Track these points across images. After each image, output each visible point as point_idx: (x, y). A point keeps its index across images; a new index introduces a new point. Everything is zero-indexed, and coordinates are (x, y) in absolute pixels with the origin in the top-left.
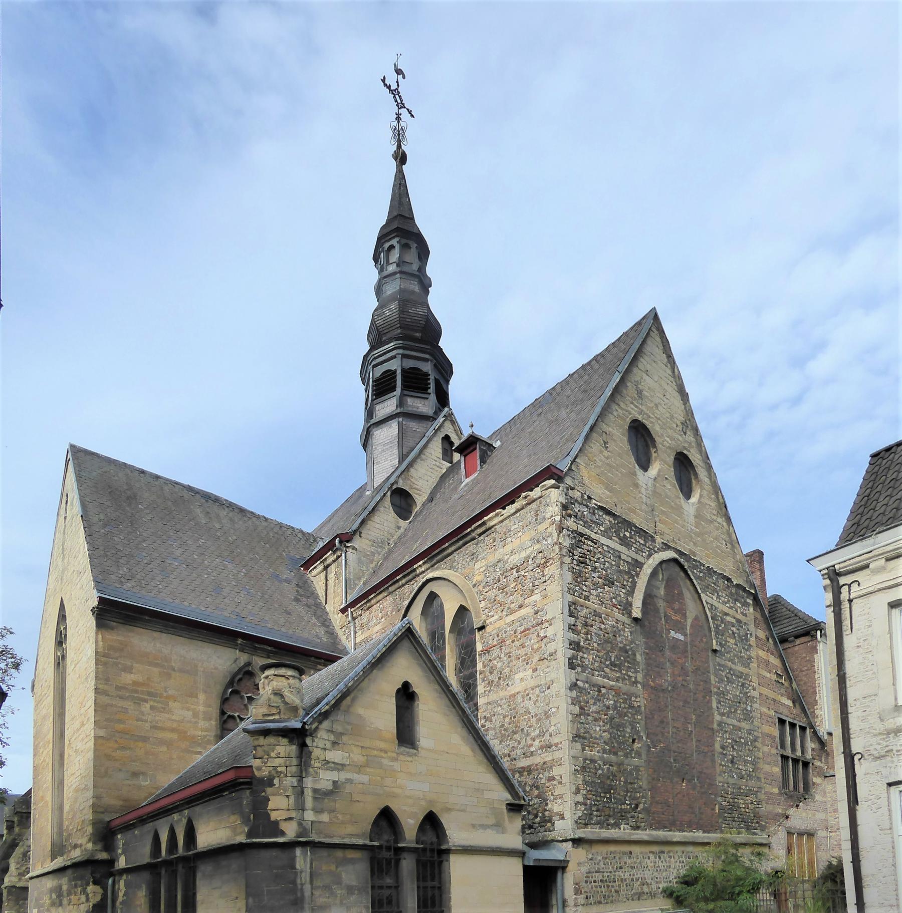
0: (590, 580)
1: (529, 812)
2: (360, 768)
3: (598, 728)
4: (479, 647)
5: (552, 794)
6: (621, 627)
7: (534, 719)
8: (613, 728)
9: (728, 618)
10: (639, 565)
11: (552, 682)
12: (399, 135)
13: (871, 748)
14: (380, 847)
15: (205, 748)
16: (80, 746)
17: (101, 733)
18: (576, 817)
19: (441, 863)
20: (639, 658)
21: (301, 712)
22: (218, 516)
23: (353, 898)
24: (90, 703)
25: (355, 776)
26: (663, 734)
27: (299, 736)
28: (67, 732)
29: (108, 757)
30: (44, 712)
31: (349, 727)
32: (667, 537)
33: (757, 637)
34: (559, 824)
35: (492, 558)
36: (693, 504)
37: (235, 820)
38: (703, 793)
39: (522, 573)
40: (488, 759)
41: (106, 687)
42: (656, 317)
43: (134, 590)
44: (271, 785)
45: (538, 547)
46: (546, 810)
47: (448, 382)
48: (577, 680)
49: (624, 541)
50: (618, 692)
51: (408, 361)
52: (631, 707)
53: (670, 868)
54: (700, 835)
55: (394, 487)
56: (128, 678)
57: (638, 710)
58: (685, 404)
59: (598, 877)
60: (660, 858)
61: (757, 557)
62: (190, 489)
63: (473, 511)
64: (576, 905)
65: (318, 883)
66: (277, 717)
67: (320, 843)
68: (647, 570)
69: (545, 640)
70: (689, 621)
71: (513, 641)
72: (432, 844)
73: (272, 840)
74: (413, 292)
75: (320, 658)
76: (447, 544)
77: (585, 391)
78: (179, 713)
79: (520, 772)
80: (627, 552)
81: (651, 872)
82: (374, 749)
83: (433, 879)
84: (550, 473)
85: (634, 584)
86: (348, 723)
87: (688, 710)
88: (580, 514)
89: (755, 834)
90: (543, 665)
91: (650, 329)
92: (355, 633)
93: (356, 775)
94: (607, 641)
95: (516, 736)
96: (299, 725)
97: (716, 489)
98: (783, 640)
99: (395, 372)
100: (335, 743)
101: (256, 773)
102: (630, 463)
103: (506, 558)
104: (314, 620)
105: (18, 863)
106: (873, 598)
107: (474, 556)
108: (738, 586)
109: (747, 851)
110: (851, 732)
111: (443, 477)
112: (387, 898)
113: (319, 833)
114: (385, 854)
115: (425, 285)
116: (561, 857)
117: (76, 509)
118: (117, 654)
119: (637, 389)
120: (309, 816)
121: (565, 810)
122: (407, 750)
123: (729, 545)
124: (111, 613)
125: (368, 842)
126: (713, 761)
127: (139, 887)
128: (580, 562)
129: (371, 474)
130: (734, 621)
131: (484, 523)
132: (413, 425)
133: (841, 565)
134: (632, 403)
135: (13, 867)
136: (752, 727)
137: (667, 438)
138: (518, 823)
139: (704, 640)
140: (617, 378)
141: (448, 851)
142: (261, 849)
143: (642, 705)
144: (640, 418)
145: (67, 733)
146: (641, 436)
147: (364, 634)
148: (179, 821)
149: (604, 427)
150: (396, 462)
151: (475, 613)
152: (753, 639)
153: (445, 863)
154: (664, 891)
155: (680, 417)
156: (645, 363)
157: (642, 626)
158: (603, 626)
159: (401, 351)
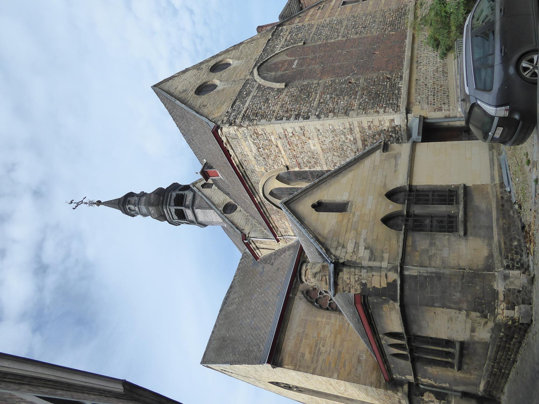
1: (389, 140)
2: (358, 234)
3: (342, 102)
4: (297, 169)
5: (379, 127)
7: (336, 138)
8: (342, 94)
9: (288, 38)
11: (316, 128)
12: (92, 203)
14: (406, 225)
15: (346, 321)
16: (342, 388)
17: (336, 375)
18: (393, 112)
19: (417, 191)
20: (305, 83)
21: (325, 263)
22: (233, 299)
23: (438, 243)
24: (320, 378)
25: (363, 237)
27: (338, 266)
29: (349, 374)
31: (335, 238)
33: (299, 22)
34: (397, 122)
35: (254, 162)
37: (386, 308)
38: (382, 42)
40: (356, 163)
42: (155, 86)
44: (365, 284)
45: (249, 138)
47: (180, 185)
50: (323, 93)
51: (171, 203)
52: (331, 85)
54: (408, 41)
56: (307, 356)
57: (333, 82)
58: (190, 70)
59: (431, 98)
61: (260, 29)
62: (221, 311)
64: (449, 110)
65: (427, 263)
66: (327, 277)
67: (401, 260)
69: (294, 133)
70: (288, 58)
71: (294, 150)
72: (405, 195)
73: (399, 288)
77: (183, 118)
78: (326, 332)
79: (365, 146)
83: (428, 196)
84: (215, 132)
86: (332, 239)
89: (409, 10)
90: (307, 134)
92: (289, 235)
93: (362, 236)
94: (296, 100)
95: (345, 148)
96: (332, 265)
97: (227, 51)
98: (301, 9)
100: (343, 247)
101: (359, 292)
104: (282, 256)
107: (253, 171)
108: (272, 35)
109: (419, 13)
111: (219, 188)
113: (395, 259)
114: (410, 223)
115: (143, 194)
118: (295, 359)
119: (182, 92)
120: (385, 264)
123: (253, 42)
124: (275, 358)
125: (402, 232)
127: (426, 371)
128: (257, 116)
129: (217, 224)
130: (289, 35)
131: (238, 166)
132: (197, 202)
136: (346, 19)
137: (204, 77)
138: (395, 146)
140: (178, 102)
141: (410, 186)
142: (403, 293)
143: (330, 79)
144: (194, 90)
145: (336, 393)
146: (203, 89)
147: (290, 231)
148: (386, 341)
152: (299, 24)
153: (418, 188)
154: (442, 58)
155: (195, 71)
157: (289, 82)
158: (288, 103)
159: (168, 206)
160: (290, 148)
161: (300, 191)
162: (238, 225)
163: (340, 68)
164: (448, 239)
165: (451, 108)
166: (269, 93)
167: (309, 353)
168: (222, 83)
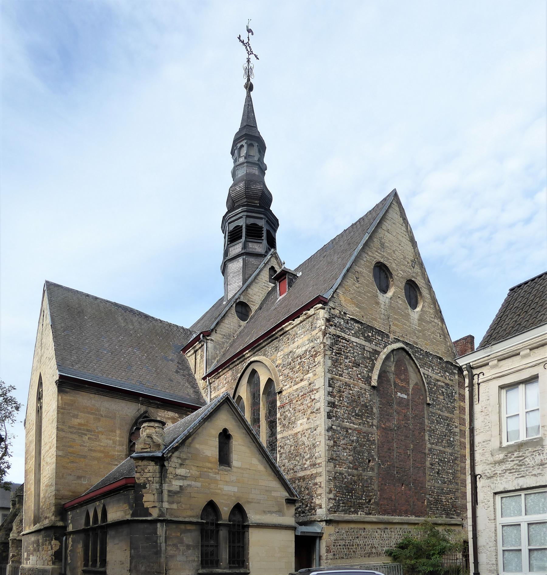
0: (343, 364)
1: (303, 504)
2: (195, 479)
3: (345, 454)
4: (278, 404)
6: (363, 392)
7: (307, 448)
9: (439, 383)
10: (378, 353)
11: (318, 426)
12: (248, 72)
13: (486, 472)
15: (120, 462)
16: (49, 460)
17: (60, 453)
18: (329, 507)
20: (375, 410)
21: (162, 447)
22: (132, 321)
23: (190, 552)
24: (54, 436)
26: (390, 457)
27: (160, 461)
28: (42, 452)
29: (64, 467)
30: (31, 439)
31: (190, 455)
32: (398, 334)
34: (319, 511)
35: (287, 350)
36: (417, 312)
37: (126, 507)
38: (416, 493)
39: (303, 360)
40: (275, 473)
41: (63, 427)
43: (80, 369)
45: (312, 344)
46: (312, 503)
48: (332, 425)
49: (368, 339)
50: (359, 432)
51: (251, 219)
52: (368, 440)
53: (393, 538)
54: (413, 518)
55: (238, 301)
56: (76, 421)
57: (373, 442)
58: (414, 248)
60: (384, 532)
62: (116, 304)
63: (310, 297)
65: (170, 542)
66: (149, 450)
67: (171, 520)
68: (383, 356)
70: (411, 386)
71: (297, 401)
72: (239, 522)
73: (144, 518)
74: (254, 174)
75: (189, 408)
76: (262, 341)
78: (105, 441)
80: (369, 346)
81: (378, 540)
82: (204, 468)
83: (239, 542)
84: (319, 300)
85: (373, 365)
86: (190, 453)
87: (408, 441)
88: (338, 324)
89: (452, 518)
90: (312, 416)
91: (392, 203)
92: (211, 392)
93: (193, 483)
94: (354, 401)
95: (297, 458)
96: (160, 455)
99: (242, 227)
100: (181, 465)
101: (137, 481)
102: (374, 290)
103: (294, 350)
104: (187, 384)
105: (17, 526)
106: (490, 383)
107: (277, 349)
110: (476, 462)
111: (269, 293)
112: (211, 552)
113: (171, 515)
114: (210, 527)
115: (263, 169)
116: (319, 531)
117: (48, 320)
118: (70, 408)
120: (166, 505)
121: (322, 503)
122: (225, 468)
124: (65, 384)
125: (200, 520)
126: (425, 473)
130: (443, 384)
132: (252, 260)
133: (474, 363)
134: (377, 252)
135: (14, 528)
137: (400, 273)
138: (292, 510)
139: (422, 398)
140: (366, 237)
141: (248, 526)
142: (139, 524)
144: (382, 261)
145: (43, 452)
146: (382, 272)
148: (99, 505)
149: (357, 269)
150: (241, 284)
151: (277, 383)
153: (246, 533)
154: (386, 552)
155: (410, 257)
156: (386, 224)
157: (378, 391)
158: (351, 392)
159: (245, 213)
160: (300, 395)
161: (242, 414)
162: (222, 324)
163: (389, 449)
164: (194, 561)
165: (329, 561)
166: (366, 367)
167: (79, 424)
168: (387, 301)
